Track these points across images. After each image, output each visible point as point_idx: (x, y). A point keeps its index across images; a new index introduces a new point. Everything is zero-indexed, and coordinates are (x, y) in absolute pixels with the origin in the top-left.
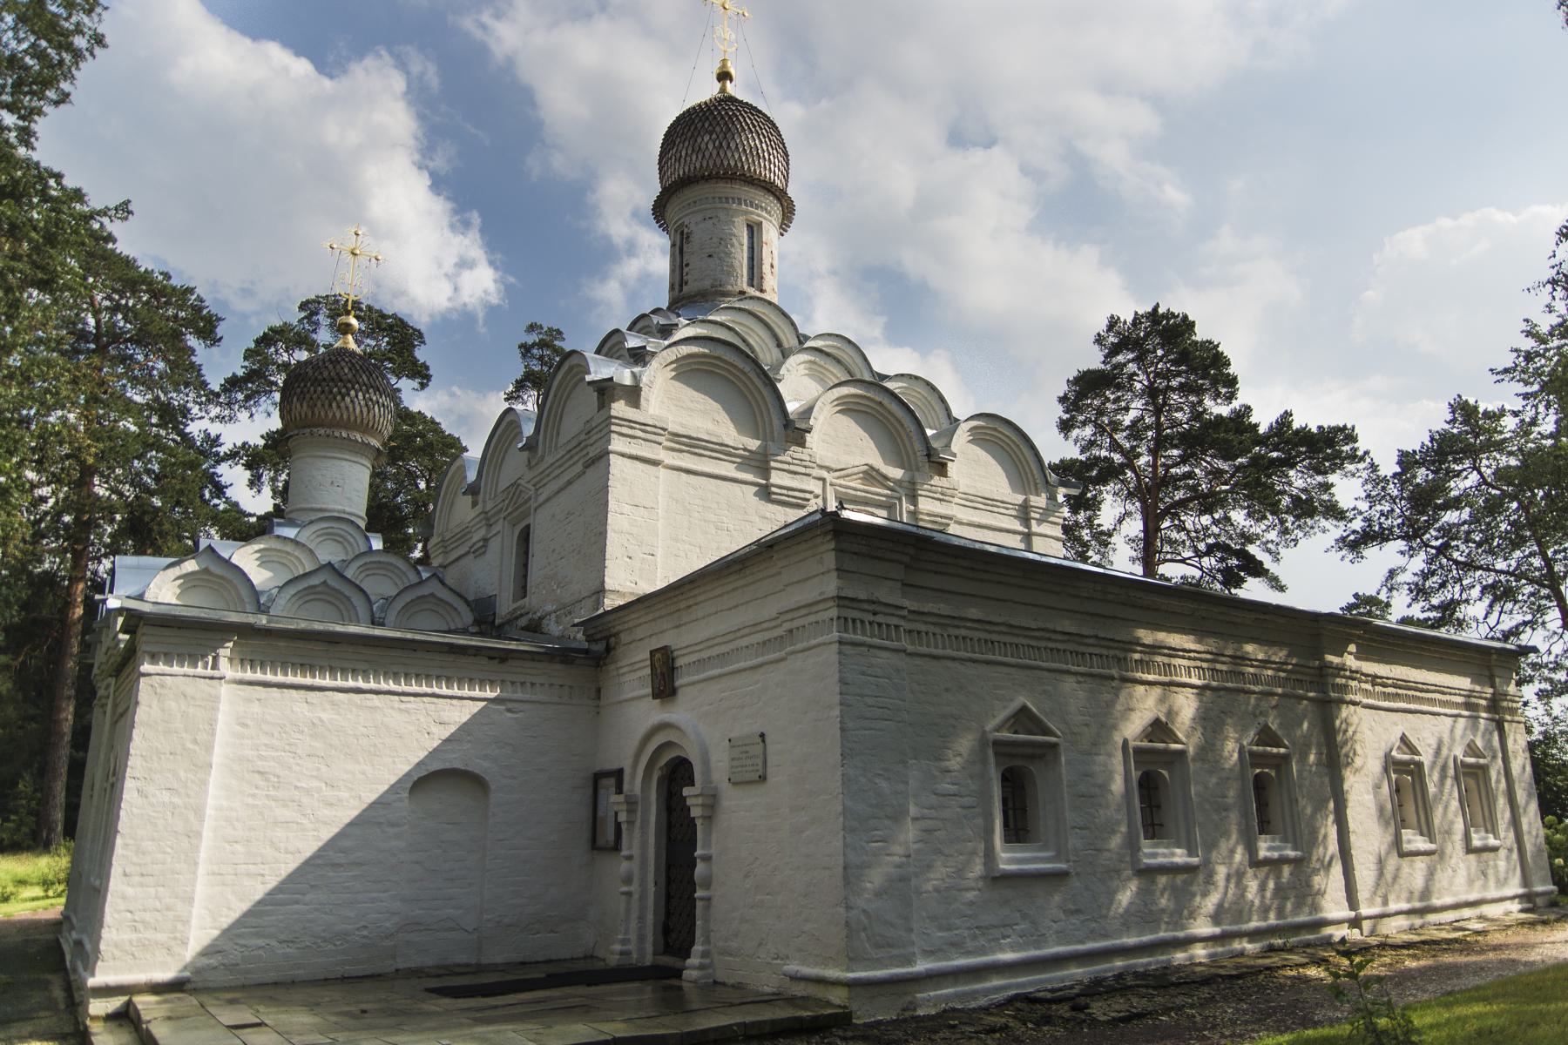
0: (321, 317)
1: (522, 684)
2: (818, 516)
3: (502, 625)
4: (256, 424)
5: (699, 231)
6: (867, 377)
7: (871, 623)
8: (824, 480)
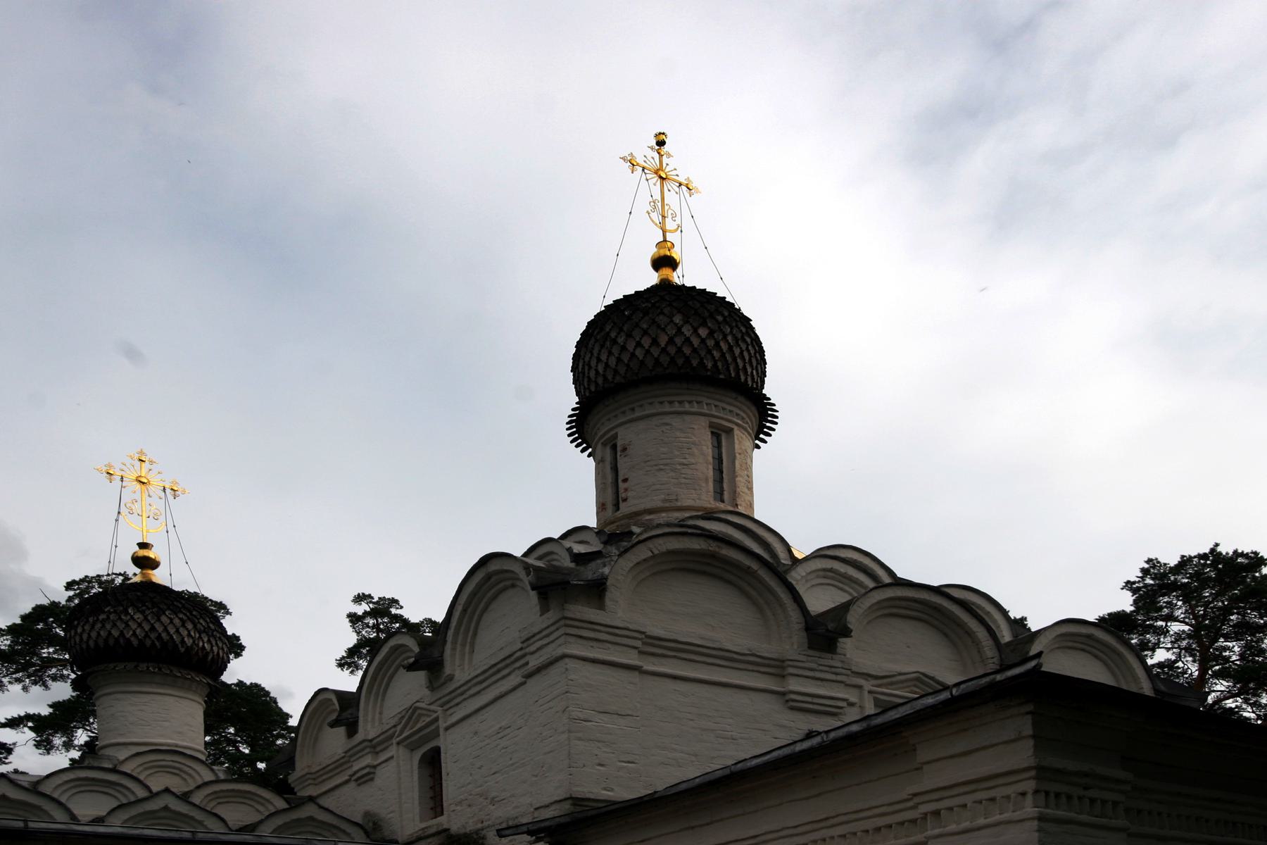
1: (1057, 795)
7: (1080, 798)
8: (860, 687)
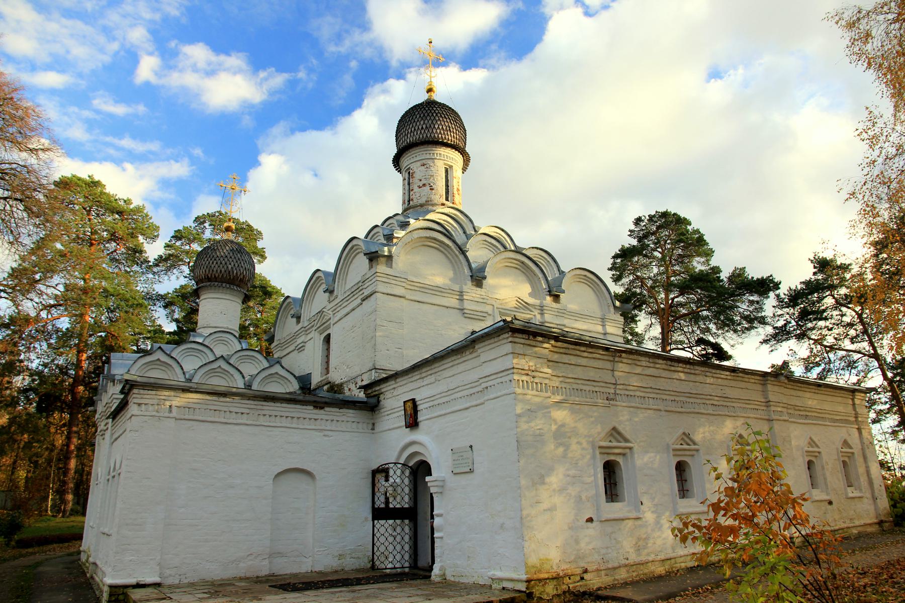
0: (207, 225)
1: (310, 419)
2: (502, 323)
3: (315, 390)
4: (174, 282)
5: (419, 172)
6: (513, 248)
